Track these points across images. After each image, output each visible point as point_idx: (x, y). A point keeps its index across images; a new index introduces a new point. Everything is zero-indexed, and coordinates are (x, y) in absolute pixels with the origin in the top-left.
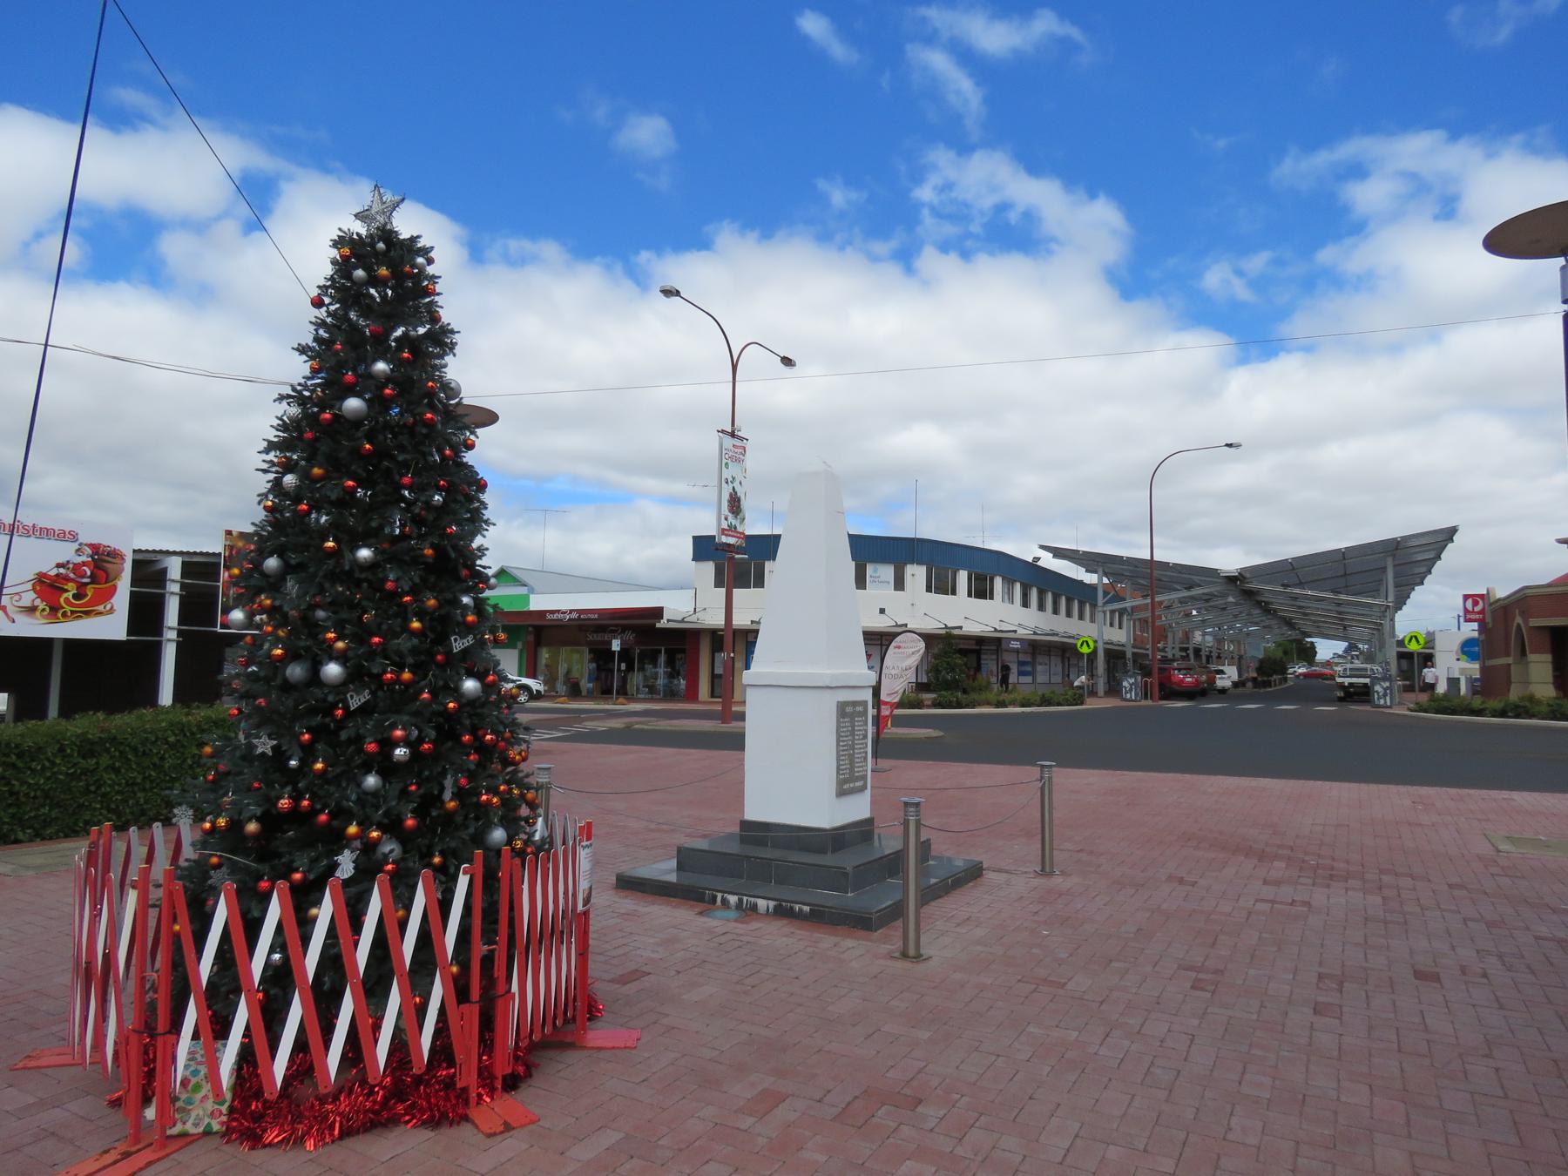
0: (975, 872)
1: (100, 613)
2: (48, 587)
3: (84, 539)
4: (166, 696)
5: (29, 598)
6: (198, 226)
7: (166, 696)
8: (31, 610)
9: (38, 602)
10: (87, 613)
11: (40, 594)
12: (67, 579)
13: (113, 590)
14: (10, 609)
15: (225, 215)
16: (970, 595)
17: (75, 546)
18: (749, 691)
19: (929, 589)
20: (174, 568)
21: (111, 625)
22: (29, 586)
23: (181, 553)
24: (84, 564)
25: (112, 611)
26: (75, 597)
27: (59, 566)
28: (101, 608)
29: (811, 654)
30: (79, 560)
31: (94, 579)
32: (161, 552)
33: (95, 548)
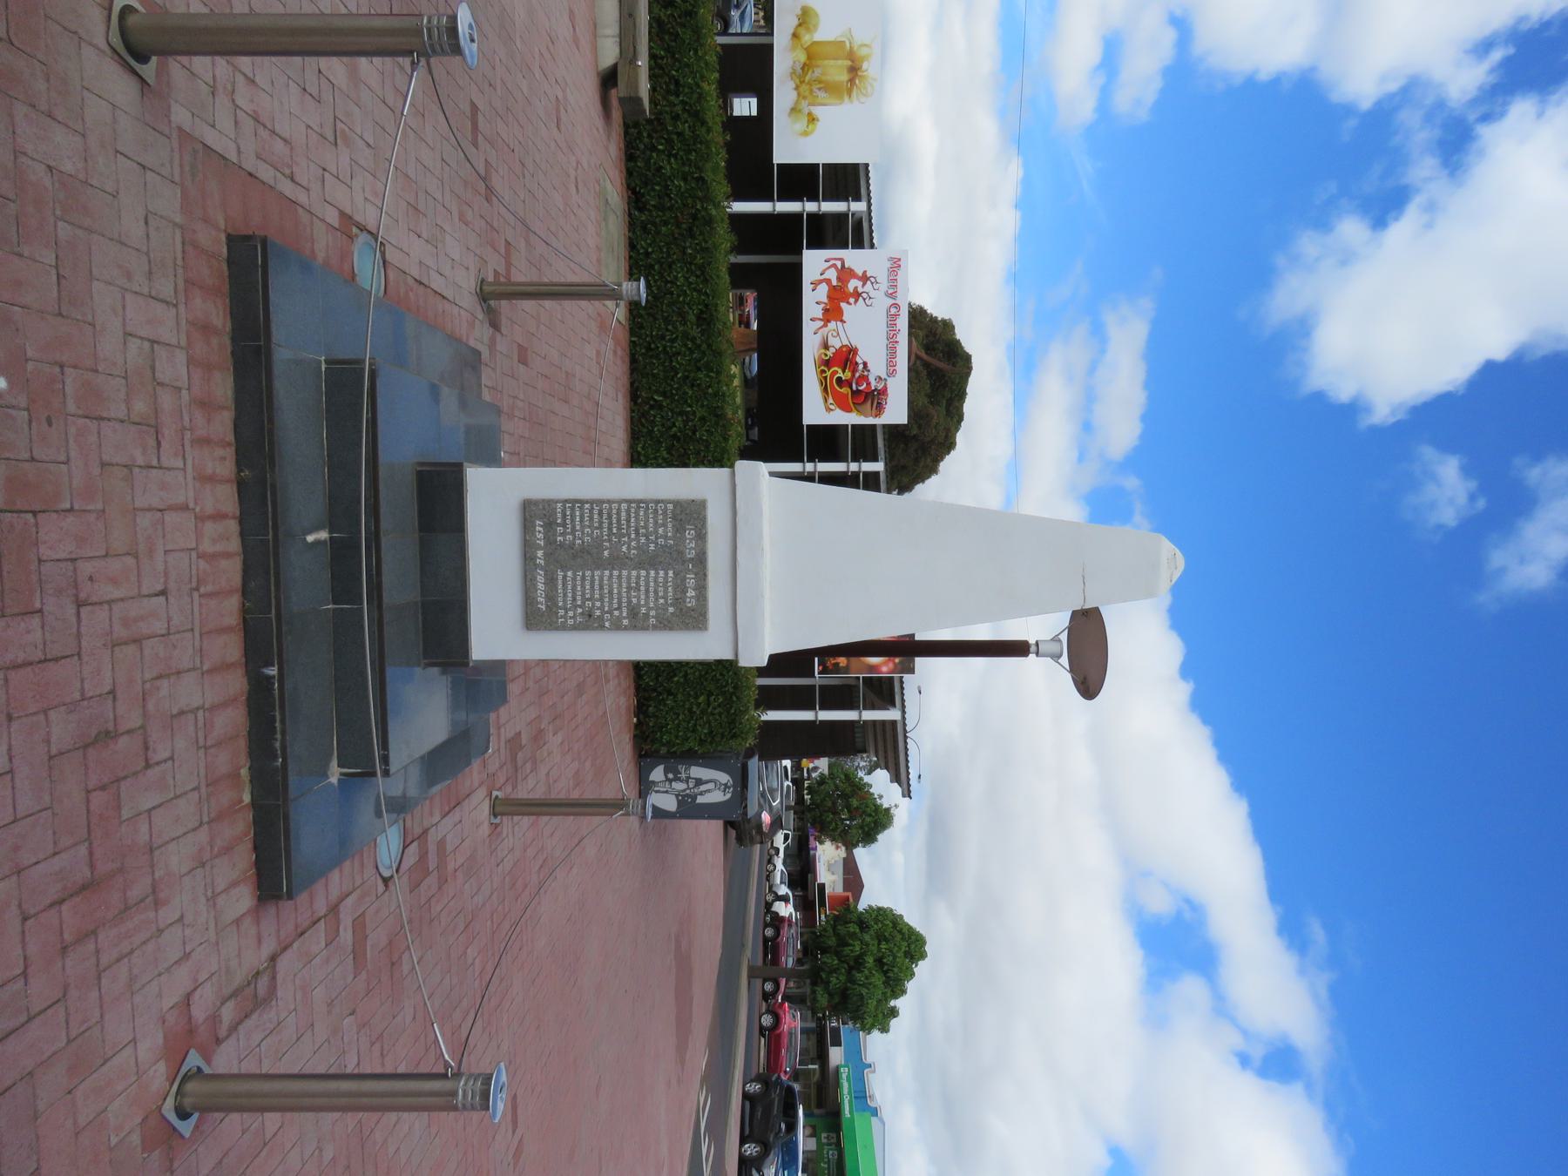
0: (273, 876)
1: (826, 400)
2: (846, 357)
3: (890, 382)
4: (740, 207)
5: (835, 343)
6: (1222, 1007)
7: (740, 207)
8: (826, 347)
9: (832, 350)
10: (825, 390)
11: (838, 352)
12: (854, 371)
13: (847, 409)
14: (825, 330)
15: (1245, 1033)
16: (867, 165)
17: (884, 376)
18: (726, 471)
19: (867, 165)
20: (858, 207)
21: (816, 410)
22: (846, 342)
23: (904, 718)
24: (869, 384)
25: (829, 410)
26: (839, 379)
27: (865, 364)
28: (831, 400)
29: (787, 563)
30: (872, 379)
31: (856, 393)
32: (903, 707)
33: (884, 392)
